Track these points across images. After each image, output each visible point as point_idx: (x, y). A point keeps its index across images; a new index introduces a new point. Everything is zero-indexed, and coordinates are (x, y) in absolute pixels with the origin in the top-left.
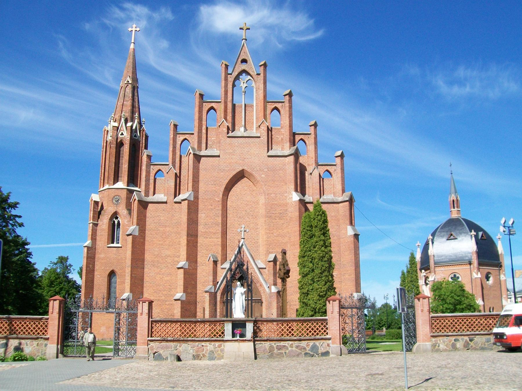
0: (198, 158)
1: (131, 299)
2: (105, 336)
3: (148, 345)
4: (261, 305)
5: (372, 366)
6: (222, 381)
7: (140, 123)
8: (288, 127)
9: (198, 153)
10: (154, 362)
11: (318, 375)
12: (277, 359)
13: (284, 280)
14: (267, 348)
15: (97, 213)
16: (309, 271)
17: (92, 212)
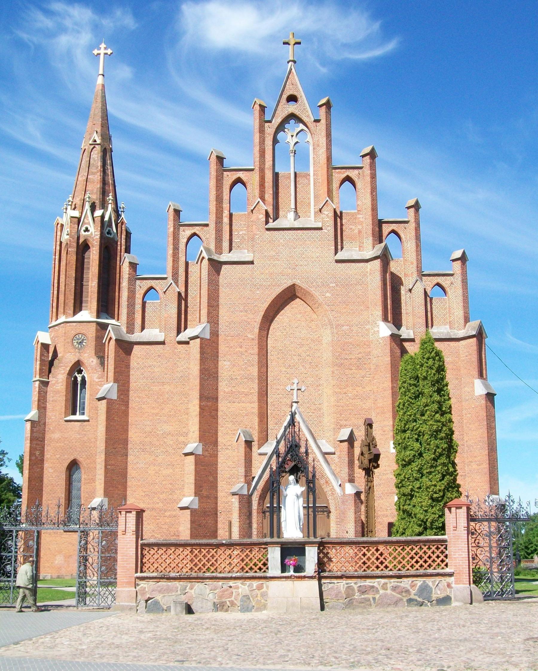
0: (216, 266)
1: (106, 507)
2: (63, 572)
3: (136, 585)
4: (328, 517)
5: (530, 622)
6: (266, 649)
7: (116, 211)
8: (369, 210)
9: (216, 257)
10: (146, 615)
11: (436, 639)
12: (359, 610)
13: (369, 472)
14: (343, 590)
15: (47, 363)
16: (414, 456)
17: (38, 363)
